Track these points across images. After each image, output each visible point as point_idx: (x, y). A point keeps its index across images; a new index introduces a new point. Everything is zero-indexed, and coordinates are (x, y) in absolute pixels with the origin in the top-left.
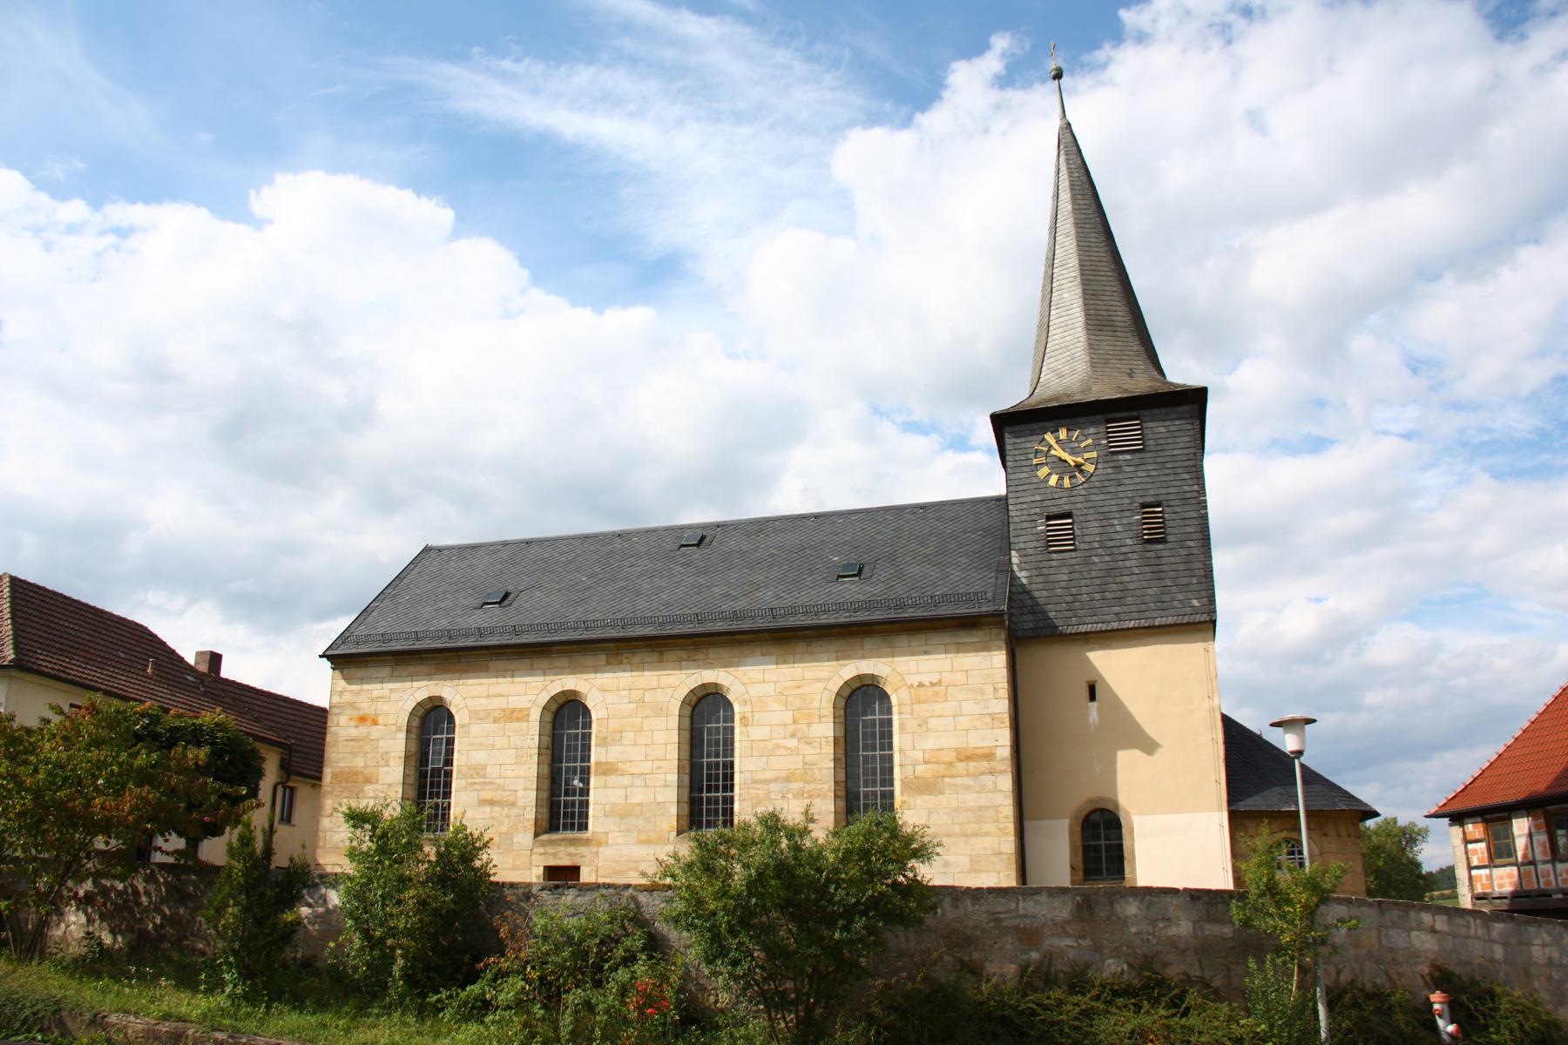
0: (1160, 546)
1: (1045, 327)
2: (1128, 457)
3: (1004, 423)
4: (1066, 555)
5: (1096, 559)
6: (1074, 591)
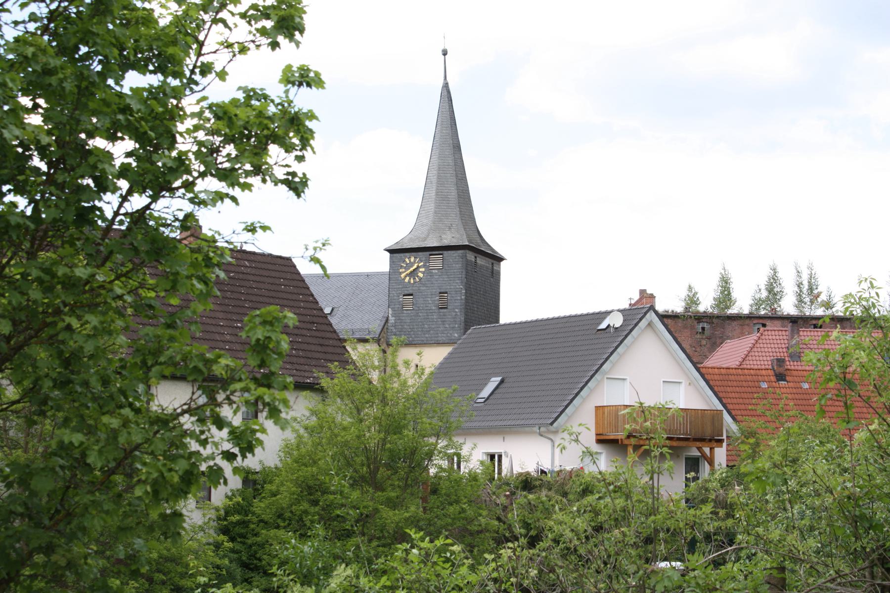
0: (445, 310)
1: (152, 267)
2: (436, 271)
3: (392, 251)
4: (409, 312)
5: (421, 314)
6: (411, 327)
